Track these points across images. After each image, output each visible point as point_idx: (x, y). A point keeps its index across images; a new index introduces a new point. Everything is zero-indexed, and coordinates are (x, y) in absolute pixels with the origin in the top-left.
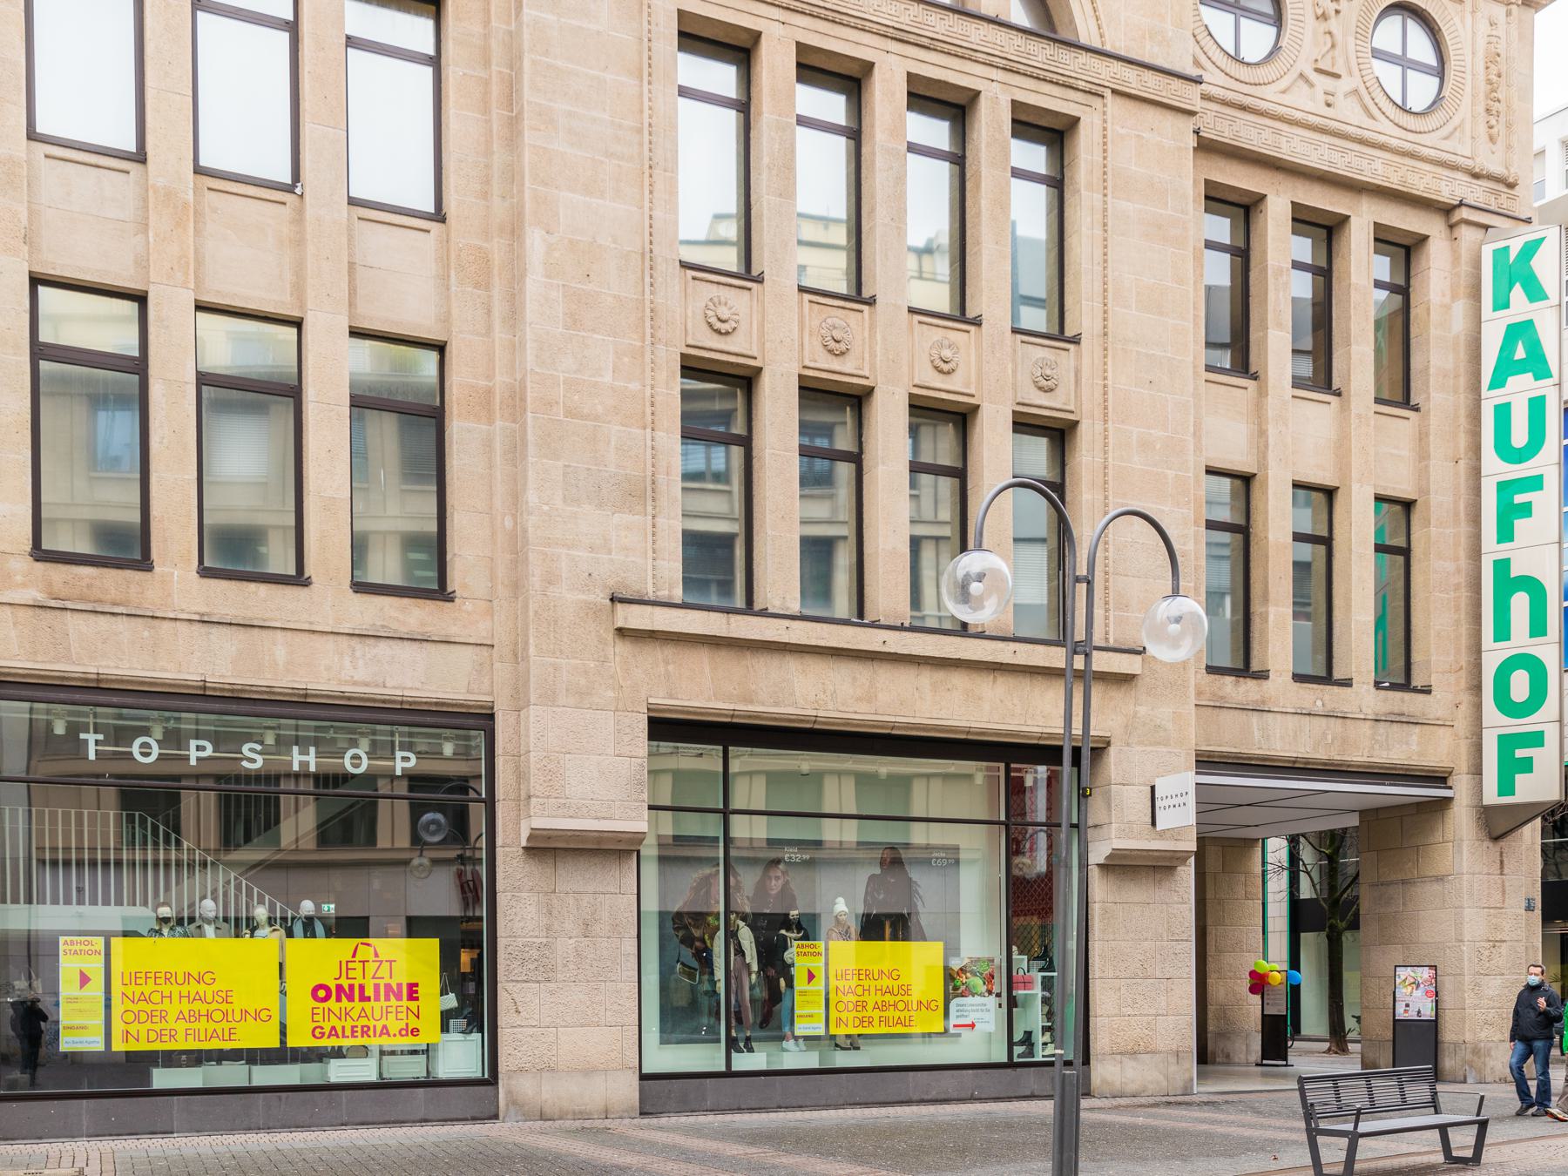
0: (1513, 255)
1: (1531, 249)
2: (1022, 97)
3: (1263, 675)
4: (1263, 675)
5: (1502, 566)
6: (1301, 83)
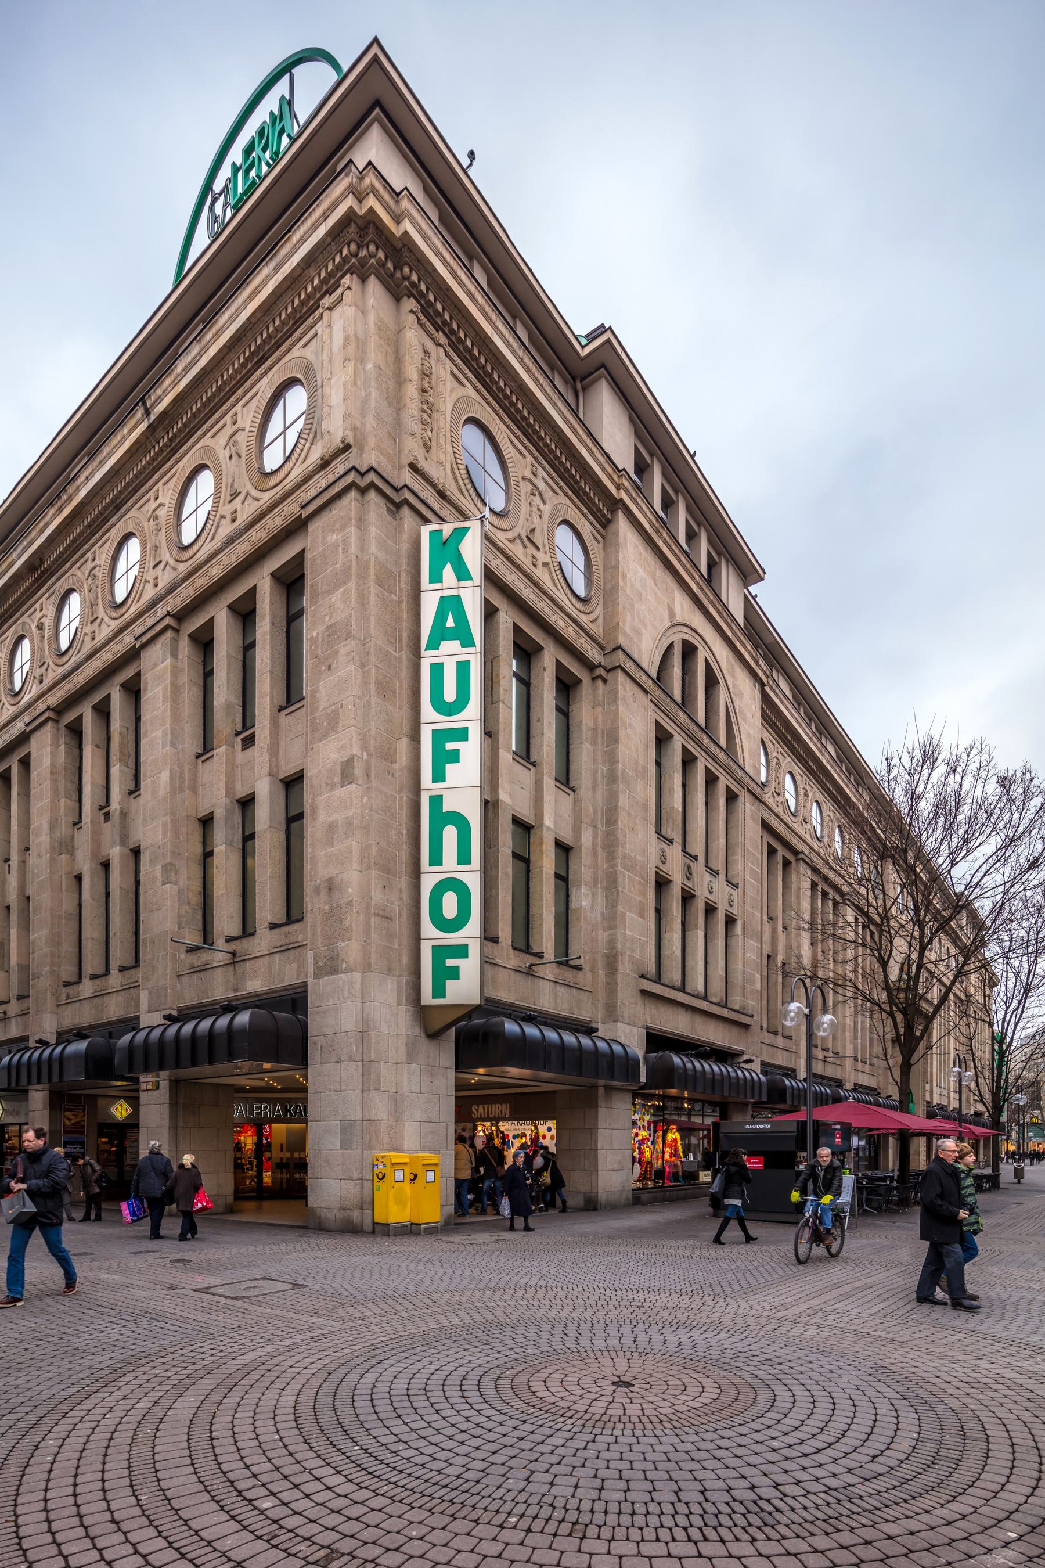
5: (436, 801)
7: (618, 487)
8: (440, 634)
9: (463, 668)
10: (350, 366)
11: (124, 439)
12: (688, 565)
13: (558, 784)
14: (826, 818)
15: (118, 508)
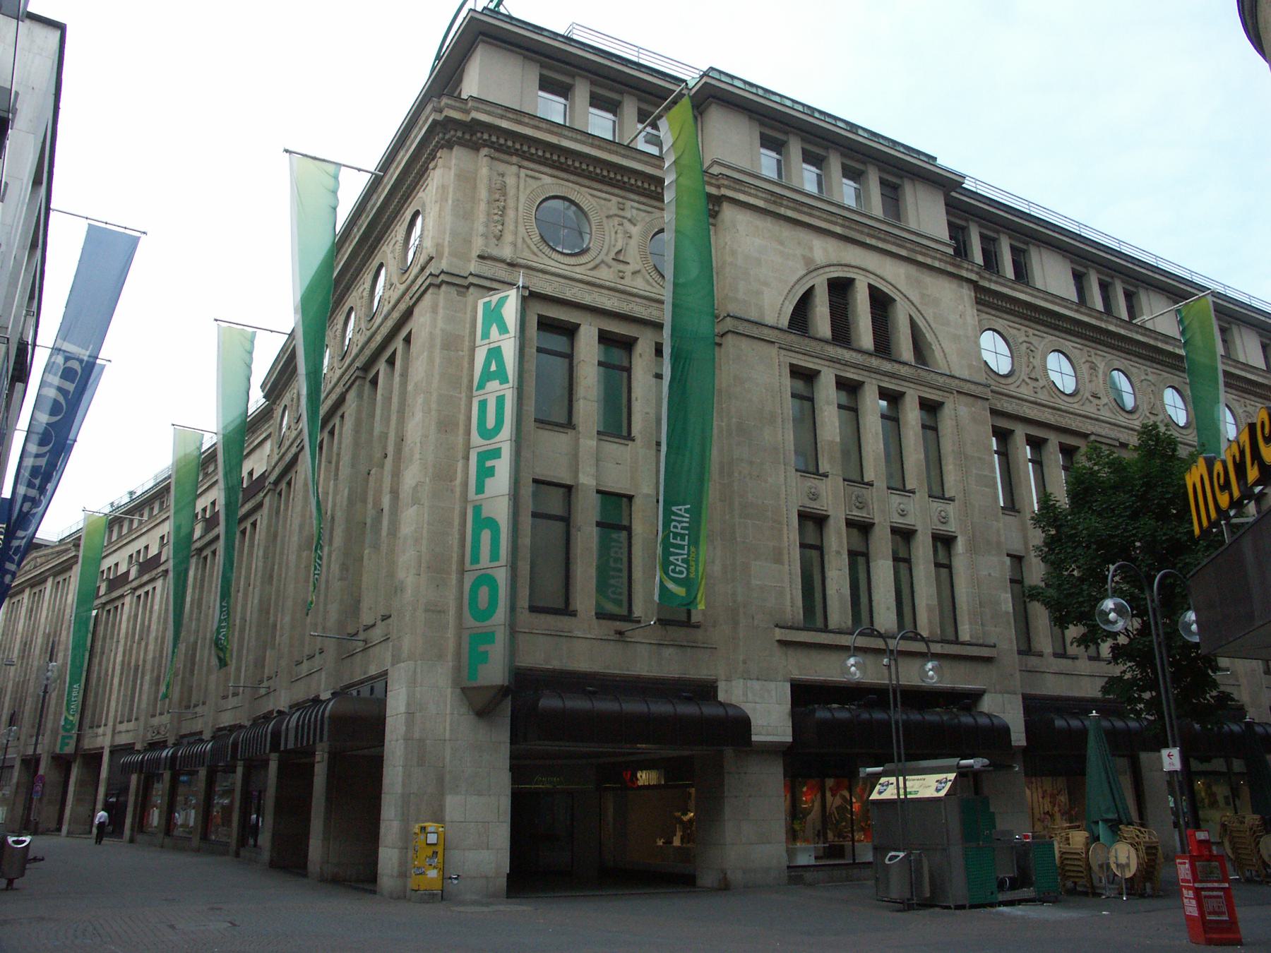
0: (493, 304)
1: (502, 301)
2: (795, 362)
3: (573, 614)
4: (573, 614)
5: (478, 509)
6: (1023, 383)
7: (719, 187)
8: (487, 376)
9: (500, 400)
10: (438, 205)
11: (347, 250)
12: (825, 216)
13: (980, 307)
14: (1137, 384)
15: (348, 289)
